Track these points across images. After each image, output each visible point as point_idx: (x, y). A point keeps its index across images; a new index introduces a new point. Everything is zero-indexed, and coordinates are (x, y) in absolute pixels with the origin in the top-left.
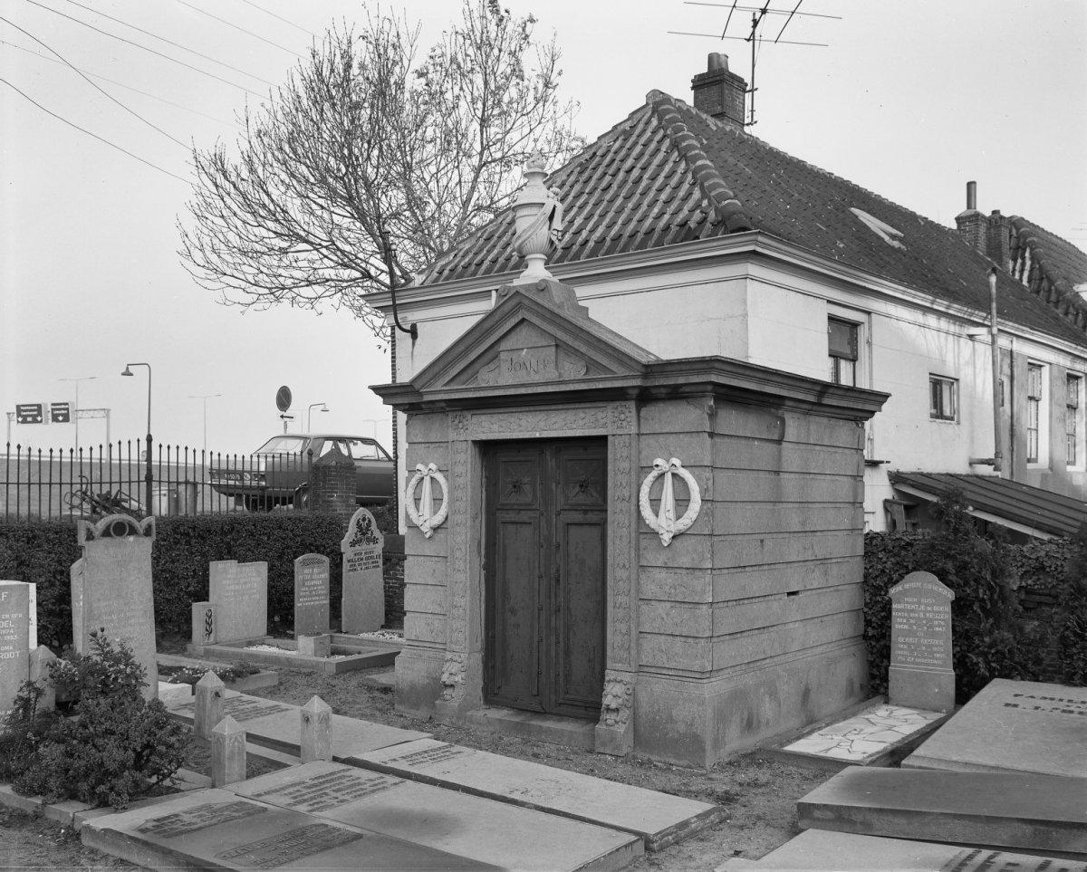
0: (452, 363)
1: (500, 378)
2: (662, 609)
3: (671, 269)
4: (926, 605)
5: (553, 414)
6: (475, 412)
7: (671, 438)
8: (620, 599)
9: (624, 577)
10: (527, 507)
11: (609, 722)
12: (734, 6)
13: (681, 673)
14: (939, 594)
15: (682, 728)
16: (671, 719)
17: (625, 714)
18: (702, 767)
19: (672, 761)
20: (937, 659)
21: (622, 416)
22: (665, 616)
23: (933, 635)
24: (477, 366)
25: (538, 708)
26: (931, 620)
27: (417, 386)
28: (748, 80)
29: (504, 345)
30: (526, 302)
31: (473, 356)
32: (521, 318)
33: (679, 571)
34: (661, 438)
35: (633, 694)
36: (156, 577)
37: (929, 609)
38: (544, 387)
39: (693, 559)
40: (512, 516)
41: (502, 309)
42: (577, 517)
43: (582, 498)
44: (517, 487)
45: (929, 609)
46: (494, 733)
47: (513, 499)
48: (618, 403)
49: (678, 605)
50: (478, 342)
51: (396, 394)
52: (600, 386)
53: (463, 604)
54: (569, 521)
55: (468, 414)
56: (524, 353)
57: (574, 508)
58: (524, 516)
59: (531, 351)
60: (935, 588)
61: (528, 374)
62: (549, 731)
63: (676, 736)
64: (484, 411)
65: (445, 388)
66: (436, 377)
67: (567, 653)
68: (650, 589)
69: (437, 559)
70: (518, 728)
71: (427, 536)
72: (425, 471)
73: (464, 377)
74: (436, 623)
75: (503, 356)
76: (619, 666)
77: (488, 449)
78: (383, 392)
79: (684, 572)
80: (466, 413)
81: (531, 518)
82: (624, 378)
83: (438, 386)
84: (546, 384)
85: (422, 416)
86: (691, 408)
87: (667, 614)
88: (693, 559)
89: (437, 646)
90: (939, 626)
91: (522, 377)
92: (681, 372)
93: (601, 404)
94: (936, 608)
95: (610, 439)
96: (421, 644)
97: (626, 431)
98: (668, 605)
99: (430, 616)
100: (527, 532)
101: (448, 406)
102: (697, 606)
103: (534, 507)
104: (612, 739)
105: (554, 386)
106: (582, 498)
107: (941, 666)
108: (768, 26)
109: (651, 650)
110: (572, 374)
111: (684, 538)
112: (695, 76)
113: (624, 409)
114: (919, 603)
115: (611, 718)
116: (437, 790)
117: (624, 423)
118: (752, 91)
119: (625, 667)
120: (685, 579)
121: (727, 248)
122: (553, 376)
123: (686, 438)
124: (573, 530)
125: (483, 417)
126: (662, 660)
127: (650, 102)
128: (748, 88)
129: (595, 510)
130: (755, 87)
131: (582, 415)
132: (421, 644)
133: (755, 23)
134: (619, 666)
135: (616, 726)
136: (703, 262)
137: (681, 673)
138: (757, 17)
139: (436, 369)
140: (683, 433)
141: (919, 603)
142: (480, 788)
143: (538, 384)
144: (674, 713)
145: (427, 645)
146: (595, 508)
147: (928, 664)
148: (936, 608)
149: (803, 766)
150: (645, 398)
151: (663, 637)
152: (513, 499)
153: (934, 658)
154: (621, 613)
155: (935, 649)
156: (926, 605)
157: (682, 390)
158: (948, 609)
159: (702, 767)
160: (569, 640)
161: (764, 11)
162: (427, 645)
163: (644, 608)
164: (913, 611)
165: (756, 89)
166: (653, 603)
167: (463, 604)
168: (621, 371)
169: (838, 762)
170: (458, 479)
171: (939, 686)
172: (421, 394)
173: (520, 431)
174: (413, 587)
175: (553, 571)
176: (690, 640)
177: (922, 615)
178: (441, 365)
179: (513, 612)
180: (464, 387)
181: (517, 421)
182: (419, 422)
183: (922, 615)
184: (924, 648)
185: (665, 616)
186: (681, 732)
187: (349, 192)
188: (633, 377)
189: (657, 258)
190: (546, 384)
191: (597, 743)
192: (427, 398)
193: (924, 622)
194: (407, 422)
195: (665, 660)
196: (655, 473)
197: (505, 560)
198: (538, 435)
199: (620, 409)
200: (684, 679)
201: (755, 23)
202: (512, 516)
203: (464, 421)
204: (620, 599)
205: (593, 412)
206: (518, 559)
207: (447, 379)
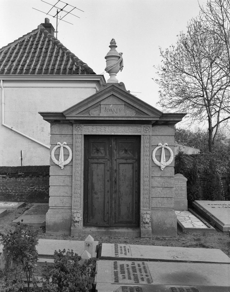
0: (81, 107)
1: (95, 114)
2: (159, 190)
3: (74, 82)
4: (180, 182)
5: (119, 127)
6: (85, 125)
7: (163, 137)
8: (145, 187)
9: (147, 180)
10: (103, 158)
11: (146, 227)
12: (54, 6)
13: (166, 209)
14: (184, 179)
15: (168, 226)
16: (165, 224)
17: (150, 225)
18: (176, 237)
19: (165, 237)
20: (183, 197)
21: (147, 129)
22: (160, 192)
23: (182, 190)
24: (90, 109)
25: (108, 225)
26: (182, 186)
27: (64, 114)
28: (55, 28)
29: (102, 103)
30: (116, 89)
31: (90, 105)
32: (111, 94)
33: (165, 178)
34: (159, 137)
35: (151, 217)
36: (219, 200)
37: (181, 183)
38: (121, 118)
39: (171, 174)
40: (96, 161)
41: (105, 90)
42: (124, 161)
43: (125, 155)
44: (98, 151)
45: (181, 183)
46: (96, 236)
47: (96, 155)
48: (145, 125)
49: (165, 188)
50: (93, 100)
51: (51, 116)
52: (144, 119)
53: (79, 192)
54: (120, 162)
55: (82, 125)
56: (111, 106)
57: (123, 158)
58: (101, 161)
59: (114, 106)
60: (181, 178)
61: (113, 113)
62: (119, 233)
63: (167, 229)
64: (89, 125)
65: (76, 115)
66: (73, 111)
67: (119, 206)
68: (155, 184)
69: (65, 176)
70: (105, 233)
71: (62, 168)
72: (62, 145)
73: (84, 112)
74: (65, 200)
75: (102, 106)
76: (145, 209)
77: (87, 137)
78: (43, 115)
79: (167, 178)
80: (81, 125)
81: (104, 161)
82: (153, 117)
83: (74, 114)
84: (122, 117)
85: (58, 125)
86: (170, 128)
87: (161, 191)
88: (171, 174)
89: (65, 208)
90: (184, 188)
91: (110, 114)
92: (172, 117)
93: (139, 125)
94: (183, 183)
95: (142, 137)
96: (57, 208)
97: (148, 134)
98: (161, 188)
99: (62, 197)
100: (102, 166)
101: (75, 122)
102: (172, 188)
103: (106, 158)
104: (148, 233)
105: (125, 118)
106: (125, 155)
107: (184, 198)
108: (61, 14)
109: (154, 203)
110: (130, 114)
111: (168, 167)
112: (51, 24)
113: (148, 127)
114: (179, 182)
115: (146, 225)
116: (219, 264)
117: (148, 132)
118: (57, 32)
119: (148, 209)
120: (168, 180)
121: (66, 78)
122: (124, 115)
123: (168, 137)
124: (121, 166)
125: (89, 127)
126: (159, 205)
127: (39, 28)
128: (55, 31)
129: (130, 159)
130: (57, 31)
131: (131, 128)
132: (57, 208)
133: (58, 13)
134: (145, 209)
135: (146, 228)
136: (82, 81)
137: (166, 209)
138: (59, 11)
139: (74, 108)
140: (167, 135)
141: (179, 182)
142: (168, 259)
143: (118, 117)
144: (166, 222)
145: (60, 208)
146: (130, 158)
147: (181, 198)
148: (183, 183)
149: (198, 232)
150: (155, 124)
151: (159, 198)
152: (96, 155)
153: (182, 196)
154: (146, 192)
155: (183, 194)
156: (180, 182)
157: (169, 122)
158: (186, 183)
159: (176, 237)
160: (120, 201)
161: (62, 10)
162: (60, 208)
163: (153, 190)
164: (177, 184)
165: (58, 32)
166: (156, 188)
167: (79, 192)
168: (152, 115)
169: (198, 229)
170: (77, 148)
171: (184, 204)
172: (65, 117)
173: (106, 132)
174: (52, 187)
175: (114, 179)
176: (169, 199)
177: (179, 185)
178: (77, 107)
179: (96, 193)
180: (82, 116)
181: (104, 129)
182: (57, 129)
183: (179, 185)
184: (180, 194)
185: (160, 192)
186: (168, 227)
187: (226, 40)
188: (157, 117)
189: (24, 78)
190: (122, 117)
191: (142, 234)
192: (67, 118)
193: (180, 187)
194: (51, 127)
195: (161, 205)
196: (158, 148)
197: (92, 175)
198: (113, 134)
199: (146, 127)
200: (167, 211)
201: (58, 13)
202: (96, 161)
203: (80, 127)
204: (145, 187)
205: (136, 127)
206: (98, 176)
207: (78, 112)
